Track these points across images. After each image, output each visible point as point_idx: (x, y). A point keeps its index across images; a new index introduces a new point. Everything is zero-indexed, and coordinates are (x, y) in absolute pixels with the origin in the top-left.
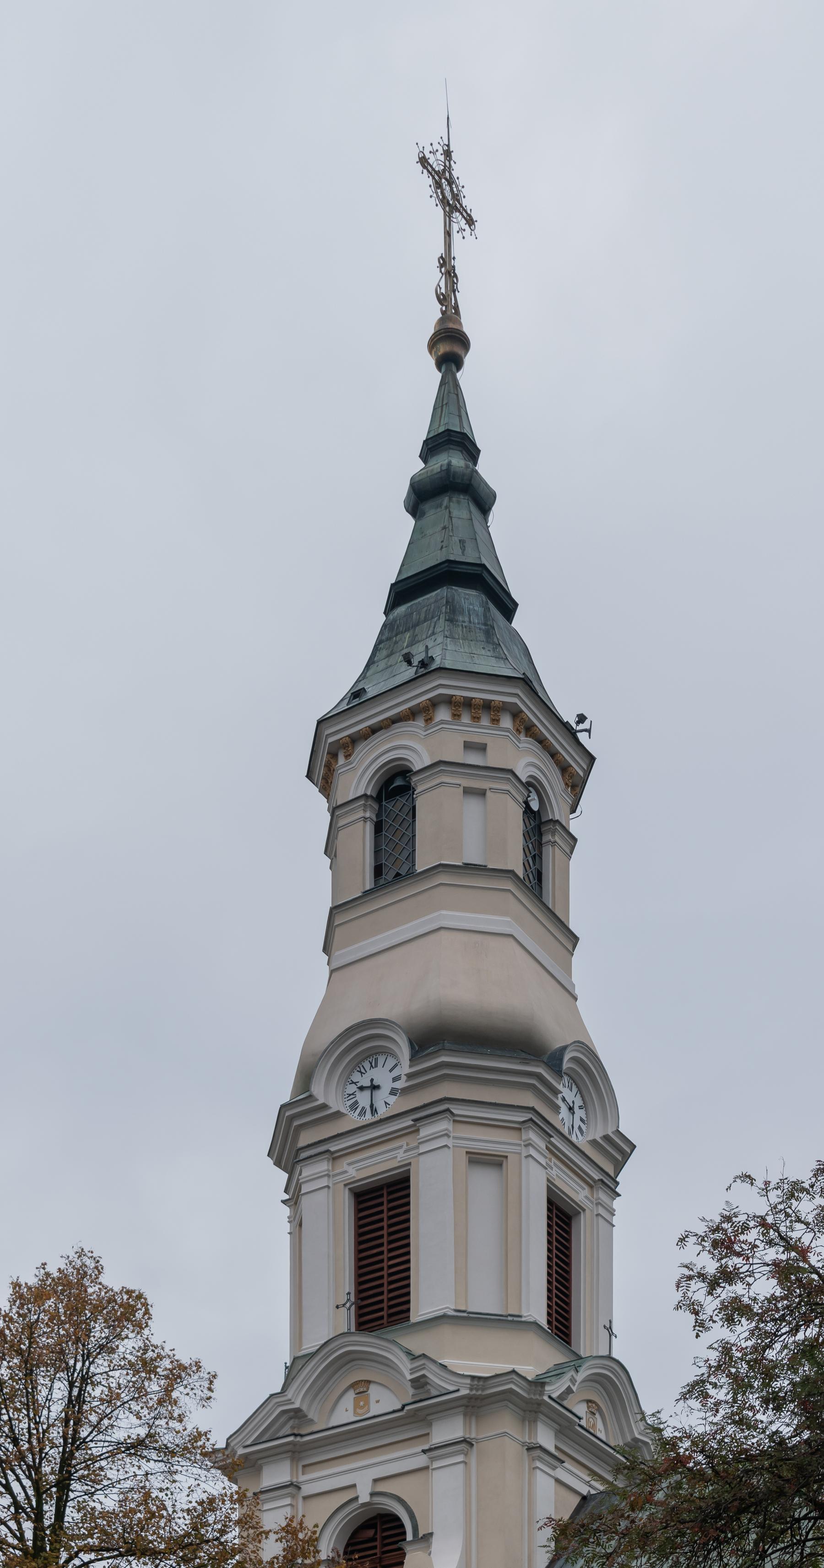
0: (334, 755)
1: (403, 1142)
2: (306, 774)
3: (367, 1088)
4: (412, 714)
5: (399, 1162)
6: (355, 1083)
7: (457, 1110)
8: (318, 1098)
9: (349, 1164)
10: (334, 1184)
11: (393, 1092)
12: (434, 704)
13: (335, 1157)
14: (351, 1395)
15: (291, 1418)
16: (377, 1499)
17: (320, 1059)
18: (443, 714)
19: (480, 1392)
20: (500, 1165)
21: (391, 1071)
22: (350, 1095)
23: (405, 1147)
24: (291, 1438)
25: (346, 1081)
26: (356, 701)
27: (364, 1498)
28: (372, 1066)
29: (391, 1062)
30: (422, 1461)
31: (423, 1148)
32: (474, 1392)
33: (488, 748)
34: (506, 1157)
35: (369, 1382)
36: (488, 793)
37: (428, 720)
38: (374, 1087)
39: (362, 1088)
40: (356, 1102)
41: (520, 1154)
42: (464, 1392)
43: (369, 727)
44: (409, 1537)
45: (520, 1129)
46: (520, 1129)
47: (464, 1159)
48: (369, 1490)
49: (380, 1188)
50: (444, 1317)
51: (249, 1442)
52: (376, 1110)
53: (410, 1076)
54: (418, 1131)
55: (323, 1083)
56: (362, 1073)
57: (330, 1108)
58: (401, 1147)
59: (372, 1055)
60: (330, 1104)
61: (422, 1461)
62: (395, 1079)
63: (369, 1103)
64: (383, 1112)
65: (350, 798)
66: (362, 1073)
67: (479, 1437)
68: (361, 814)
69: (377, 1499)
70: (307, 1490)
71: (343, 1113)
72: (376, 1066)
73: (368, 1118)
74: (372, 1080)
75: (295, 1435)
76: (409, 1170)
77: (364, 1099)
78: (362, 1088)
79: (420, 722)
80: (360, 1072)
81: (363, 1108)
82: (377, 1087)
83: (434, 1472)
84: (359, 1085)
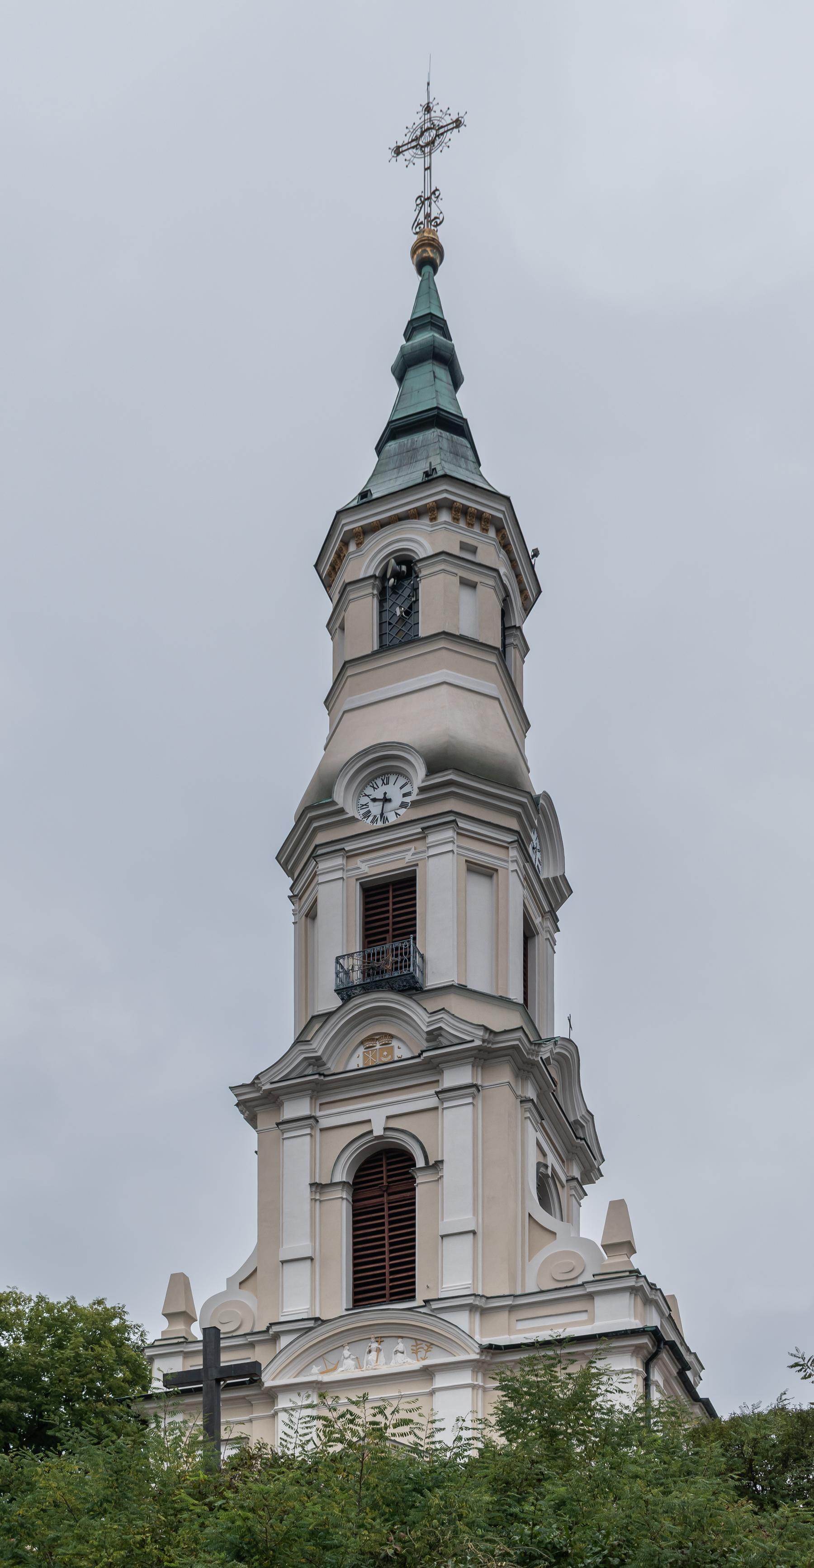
0: (345, 543)
1: (412, 846)
2: (314, 563)
3: (379, 800)
4: (417, 514)
5: (407, 863)
6: (368, 796)
7: (462, 824)
8: (338, 803)
9: (363, 862)
10: (348, 878)
11: (403, 805)
12: (439, 506)
13: (349, 856)
14: (361, 1050)
15: (310, 1065)
16: (389, 1134)
17: (341, 771)
18: (444, 517)
19: (490, 1045)
20: (490, 876)
21: (401, 788)
22: (363, 805)
23: (413, 851)
24: (317, 1077)
25: (360, 794)
26: (365, 500)
27: (378, 1131)
28: (383, 783)
29: (402, 781)
30: (433, 1102)
31: (432, 852)
32: (486, 1044)
33: (479, 550)
34: (497, 870)
35: (392, 1036)
36: (479, 586)
37: (433, 519)
38: (386, 800)
39: (374, 800)
40: (369, 812)
41: (507, 869)
42: (478, 1043)
43: (379, 521)
44: (420, 1163)
45: (507, 848)
46: (507, 848)
47: (464, 866)
48: (383, 1126)
49: (386, 885)
50: (452, 986)
51: (276, 1079)
52: (387, 819)
53: (422, 790)
54: (424, 838)
55: (343, 789)
56: (374, 788)
57: (347, 813)
58: (409, 850)
59: (384, 774)
60: (347, 810)
61: (433, 1102)
62: (405, 795)
63: (380, 812)
64: (392, 819)
65: (361, 576)
66: (374, 788)
67: (485, 1084)
68: (370, 591)
69: (389, 1134)
70: (325, 1123)
71: (357, 819)
72: (388, 783)
73: (380, 824)
74: (385, 794)
75: (320, 1074)
76: (415, 871)
77: (375, 809)
78: (374, 800)
79: (426, 521)
80: (373, 787)
81: (375, 816)
82: (389, 800)
83: (445, 1111)
84: (371, 797)
